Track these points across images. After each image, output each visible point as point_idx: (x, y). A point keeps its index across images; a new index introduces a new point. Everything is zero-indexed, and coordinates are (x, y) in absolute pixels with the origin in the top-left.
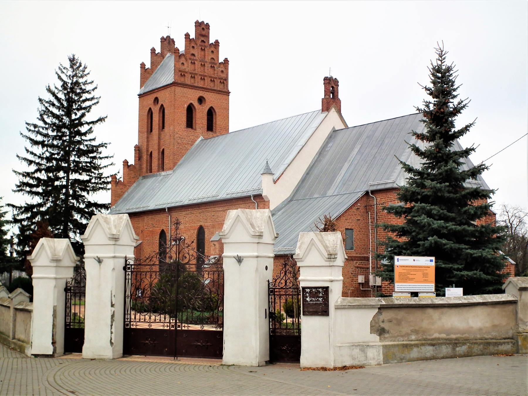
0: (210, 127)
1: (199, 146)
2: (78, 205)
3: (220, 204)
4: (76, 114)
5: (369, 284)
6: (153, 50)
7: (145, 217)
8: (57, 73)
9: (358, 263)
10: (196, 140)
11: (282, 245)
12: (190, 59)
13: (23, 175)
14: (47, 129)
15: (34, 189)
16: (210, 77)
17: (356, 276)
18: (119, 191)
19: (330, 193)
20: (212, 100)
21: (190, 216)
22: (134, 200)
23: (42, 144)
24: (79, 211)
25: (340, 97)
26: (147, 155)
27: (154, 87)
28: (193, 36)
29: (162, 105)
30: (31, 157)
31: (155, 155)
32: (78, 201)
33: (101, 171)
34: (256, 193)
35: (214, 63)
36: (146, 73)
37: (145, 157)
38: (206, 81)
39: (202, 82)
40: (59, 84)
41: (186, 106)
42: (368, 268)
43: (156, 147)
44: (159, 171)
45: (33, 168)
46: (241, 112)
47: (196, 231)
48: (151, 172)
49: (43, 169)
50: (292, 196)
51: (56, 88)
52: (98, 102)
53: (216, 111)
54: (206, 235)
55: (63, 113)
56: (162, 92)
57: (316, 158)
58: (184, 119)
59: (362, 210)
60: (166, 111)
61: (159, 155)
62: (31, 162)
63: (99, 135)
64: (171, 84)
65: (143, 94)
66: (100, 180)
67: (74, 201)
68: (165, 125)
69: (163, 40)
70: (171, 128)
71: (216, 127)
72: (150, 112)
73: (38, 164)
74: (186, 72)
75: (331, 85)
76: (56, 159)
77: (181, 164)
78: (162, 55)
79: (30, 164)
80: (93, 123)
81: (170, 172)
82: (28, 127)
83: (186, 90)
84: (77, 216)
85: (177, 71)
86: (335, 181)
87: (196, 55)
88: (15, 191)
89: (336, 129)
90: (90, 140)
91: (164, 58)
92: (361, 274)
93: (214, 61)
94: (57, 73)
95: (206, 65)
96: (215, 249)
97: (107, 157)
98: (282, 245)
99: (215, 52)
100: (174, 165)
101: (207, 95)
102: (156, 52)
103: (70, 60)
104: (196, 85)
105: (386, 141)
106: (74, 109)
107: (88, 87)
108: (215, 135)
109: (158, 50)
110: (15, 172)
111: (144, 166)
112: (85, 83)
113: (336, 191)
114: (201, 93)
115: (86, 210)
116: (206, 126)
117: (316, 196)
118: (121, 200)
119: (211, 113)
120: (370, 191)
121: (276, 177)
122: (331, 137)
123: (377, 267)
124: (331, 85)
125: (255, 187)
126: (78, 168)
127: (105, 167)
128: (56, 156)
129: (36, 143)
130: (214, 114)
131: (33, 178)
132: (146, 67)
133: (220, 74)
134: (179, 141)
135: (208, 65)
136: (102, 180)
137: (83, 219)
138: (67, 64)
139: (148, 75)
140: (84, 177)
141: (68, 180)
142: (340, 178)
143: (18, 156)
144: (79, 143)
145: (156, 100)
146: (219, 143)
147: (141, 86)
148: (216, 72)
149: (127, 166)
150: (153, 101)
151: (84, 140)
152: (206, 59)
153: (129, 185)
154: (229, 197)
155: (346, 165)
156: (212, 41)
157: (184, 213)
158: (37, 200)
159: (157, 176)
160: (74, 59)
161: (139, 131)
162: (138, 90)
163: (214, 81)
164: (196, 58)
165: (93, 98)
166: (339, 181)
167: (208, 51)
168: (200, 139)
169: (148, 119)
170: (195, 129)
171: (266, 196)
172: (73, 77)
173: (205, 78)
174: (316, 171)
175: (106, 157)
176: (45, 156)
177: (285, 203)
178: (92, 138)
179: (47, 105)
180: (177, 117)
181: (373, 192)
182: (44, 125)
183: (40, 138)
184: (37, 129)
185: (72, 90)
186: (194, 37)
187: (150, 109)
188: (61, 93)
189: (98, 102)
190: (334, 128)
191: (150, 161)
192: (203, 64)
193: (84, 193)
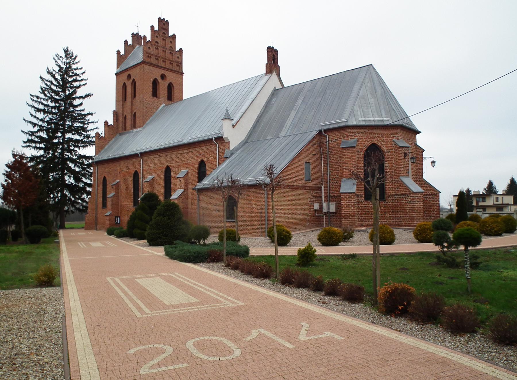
1: (162, 110)
4: (69, 91)
6: (126, 42)
7: (122, 162)
8: (54, 59)
9: (313, 193)
11: (252, 175)
12: (155, 45)
13: (30, 135)
14: (47, 100)
15: (38, 145)
16: (169, 60)
17: (313, 203)
19: (282, 134)
20: (171, 77)
23: (44, 111)
26: (123, 117)
27: (127, 67)
28: (156, 28)
29: (134, 80)
30: (35, 121)
31: (129, 117)
32: (71, 154)
33: (88, 133)
35: (172, 50)
36: (120, 59)
40: (57, 69)
42: (321, 197)
43: (129, 111)
44: (131, 129)
45: (36, 129)
49: (45, 130)
51: (54, 70)
52: (86, 84)
53: (175, 86)
54: (172, 174)
56: (134, 69)
61: (131, 117)
62: (35, 125)
63: (87, 106)
68: (137, 94)
70: (141, 96)
72: (125, 86)
73: (40, 126)
74: (152, 55)
75: (272, 54)
76: (54, 123)
77: (148, 124)
78: (133, 46)
79: (34, 127)
82: (32, 98)
83: (152, 68)
84: (71, 165)
85: (145, 53)
88: (24, 147)
90: (80, 111)
91: (134, 48)
92: (316, 202)
94: (54, 59)
97: (93, 122)
98: (252, 175)
100: (143, 124)
101: (167, 73)
102: (129, 44)
103: (64, 51)
104: (159, 65)
107: (78, 72)
108: (174, 103)
109: (130, 42)
110: (23, 132)
111: (121, 126)
113: (288, 133)
114: (162, 72)
117: (269, 137)
119: (170, 87)
120: (323, 130)
121: (234, 122)
124: (272, 54)
125: (216, 131)
126: (71, 129)
128: (55, 121)
129: (38, 110)
131: (37, 137)
133: (177, 59)
136: (90, 139)
138: (63, 54)
140: (77, 137)
143: (24, 120)
145: (129, 76)
146: (177, 107)
147: (117, 68)
154: (192, 141)
155: (293, 114)
156: (170, 34)
157: (153, 157)
158: (41, 152)
159: (130, 133)
160: (67, 50)
161: (116, 101)
162: (115, 71)
165: (82, 80)
166: (289, 125)
168: (162, 106)
170: (159, 98)
171: (227, 138)
174: (265, 119)
175: (92, 122)
176: (46, 120)
179: (48, 84)
181: (326, 131)
182: (44, 97)
183: (41, 107)
184: (39, 100)
187: (125, 83)
189: (86, 84)
191: (125, 120)
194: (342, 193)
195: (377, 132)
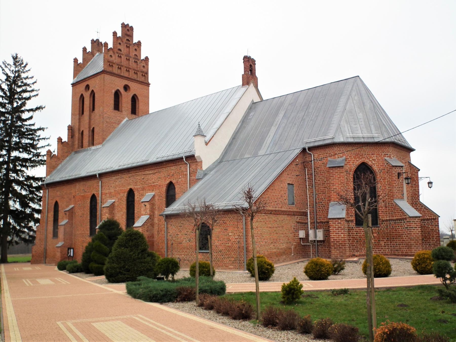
0: (134, 111)
1: (124, 125)
2: (18, 178)
3: (150, 168)
4: (17, 103)
5: (308, 239)
6: (85, 49)
7: (77, 184)
10: (122, 121)
12: (117, 53)
16: (134, 70)
17: (297, 231)
18: (54, 163)
19: (261, 152)
20: (135, 88)
21: (120, 180)
22: (67, 170)
24: (19, 183)
25: (257, 74)
26: (79, 133)
27: (86, 76)
28: (119, 34)
29: (93, 91)
31: (86, 133)
32: (18, 175)
34: (188, 154)
37: (77, 135)
38: (130, 73)
39: (127, 73)
41: (114, 91)
42: (307, 223)
43: (87, 126)
44: (89, 146)
46: (159, 97)
47: (126, 193)
48: (82, 148)
50: (221, 157)
52: (37, 95)
54: (136, 197)
55: (7, 102)
57: (240, 125)
58: (112, 102)
59: (300, 166)
60: (96, 96)
63: (37, 121)
64: (101, 72)
65: (76, 82)
66: (38, 157)
67: (14, 175)
68: (96, 107)
69: (93, 42)
71: (138, 111)
72: (82, 97)
74: (114, 64)
75: (249, 64)
77: (109, 139)
78: (92, 54)
80: (32, 110)
81: (100, 146)
84: (17, 188)
85: (106, 61)
86: (265, 143)
87: (122, 50)
89: (255, 102)
90: (30, 125)
91: (93, 56)
92: (301, 230)
93: (137, 57)
95: (130, 59)
96: (146, 209)
97: (44, 139)
99: (138, 50)
100: (103, 141)
102: (88, 51)
104: (122, 74)
105: (312, 106)
106: (16, 99)
107: (28, 81)
108: (139, 116)
109: (89, 49)
111: (76, 142)
112: (27, 78)
115: (25, 183)
116: (130, 110)
117: (247, 156)
118: (55, 171)
119: (134, 99)
120: (307, 148)
121: (207, 139)
122: (251, 108)
123: (317, 222)
124: (249, 64)
125: (186, 149)
126: (18, 146)
127: (42, 147)
130: (137, 100)
132: (79, 62)
133: (142, 68)
134: (108, 120)
135: (132, 60)
137: (22, 190)
138: (11, 62)
139: (80, 68)
140: (24, 155)
141: (9, 157)
142: (270, 140)
144: (21, 127)
145: (88, 87)
146: (141, 122)
147: (74, 77)
148: (138, 66)
149: (60, 143)
150: (84, 88)
151: (24, 125)
152: (131, 55)
153: (62, 158)
154: (159, 160)
155: (273, 129)
157: (114, 178)
159: (87, 150)
160: (17, 57)
161: (72, 114)
162: (71, 80)
163: (137, 73)
164: (122, 52)
165: (33, 91)
166: (269, 142)
167: (132, 49)
168: (125, 120)
169: (80, 103)
170: (122, 112)
172: (16, 72)
173: (130, 70)
174: (242, 136)
175: (43, 139)
177: (216, 164)
178: (31, 123)
180: (105, 101)
181: (310, 149)
185: (15, 82)
186: (121, 35)
187: (82, 95)
188: (4, 84)
189: (37, 95)
190: (253, 100)
191: (81, 138)
192: (128, 58)
193: (23, 169)
194: (330, 219)
195: (366, 149)
